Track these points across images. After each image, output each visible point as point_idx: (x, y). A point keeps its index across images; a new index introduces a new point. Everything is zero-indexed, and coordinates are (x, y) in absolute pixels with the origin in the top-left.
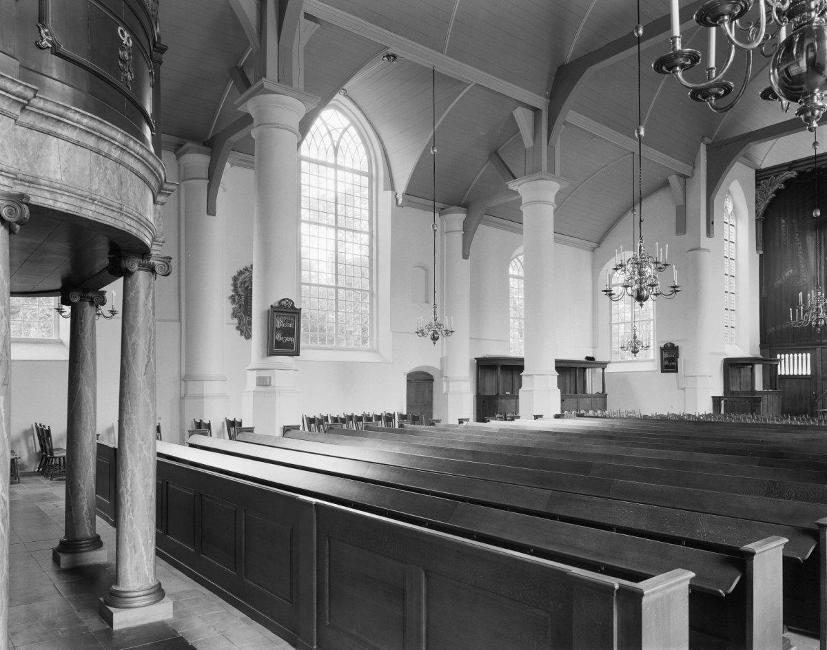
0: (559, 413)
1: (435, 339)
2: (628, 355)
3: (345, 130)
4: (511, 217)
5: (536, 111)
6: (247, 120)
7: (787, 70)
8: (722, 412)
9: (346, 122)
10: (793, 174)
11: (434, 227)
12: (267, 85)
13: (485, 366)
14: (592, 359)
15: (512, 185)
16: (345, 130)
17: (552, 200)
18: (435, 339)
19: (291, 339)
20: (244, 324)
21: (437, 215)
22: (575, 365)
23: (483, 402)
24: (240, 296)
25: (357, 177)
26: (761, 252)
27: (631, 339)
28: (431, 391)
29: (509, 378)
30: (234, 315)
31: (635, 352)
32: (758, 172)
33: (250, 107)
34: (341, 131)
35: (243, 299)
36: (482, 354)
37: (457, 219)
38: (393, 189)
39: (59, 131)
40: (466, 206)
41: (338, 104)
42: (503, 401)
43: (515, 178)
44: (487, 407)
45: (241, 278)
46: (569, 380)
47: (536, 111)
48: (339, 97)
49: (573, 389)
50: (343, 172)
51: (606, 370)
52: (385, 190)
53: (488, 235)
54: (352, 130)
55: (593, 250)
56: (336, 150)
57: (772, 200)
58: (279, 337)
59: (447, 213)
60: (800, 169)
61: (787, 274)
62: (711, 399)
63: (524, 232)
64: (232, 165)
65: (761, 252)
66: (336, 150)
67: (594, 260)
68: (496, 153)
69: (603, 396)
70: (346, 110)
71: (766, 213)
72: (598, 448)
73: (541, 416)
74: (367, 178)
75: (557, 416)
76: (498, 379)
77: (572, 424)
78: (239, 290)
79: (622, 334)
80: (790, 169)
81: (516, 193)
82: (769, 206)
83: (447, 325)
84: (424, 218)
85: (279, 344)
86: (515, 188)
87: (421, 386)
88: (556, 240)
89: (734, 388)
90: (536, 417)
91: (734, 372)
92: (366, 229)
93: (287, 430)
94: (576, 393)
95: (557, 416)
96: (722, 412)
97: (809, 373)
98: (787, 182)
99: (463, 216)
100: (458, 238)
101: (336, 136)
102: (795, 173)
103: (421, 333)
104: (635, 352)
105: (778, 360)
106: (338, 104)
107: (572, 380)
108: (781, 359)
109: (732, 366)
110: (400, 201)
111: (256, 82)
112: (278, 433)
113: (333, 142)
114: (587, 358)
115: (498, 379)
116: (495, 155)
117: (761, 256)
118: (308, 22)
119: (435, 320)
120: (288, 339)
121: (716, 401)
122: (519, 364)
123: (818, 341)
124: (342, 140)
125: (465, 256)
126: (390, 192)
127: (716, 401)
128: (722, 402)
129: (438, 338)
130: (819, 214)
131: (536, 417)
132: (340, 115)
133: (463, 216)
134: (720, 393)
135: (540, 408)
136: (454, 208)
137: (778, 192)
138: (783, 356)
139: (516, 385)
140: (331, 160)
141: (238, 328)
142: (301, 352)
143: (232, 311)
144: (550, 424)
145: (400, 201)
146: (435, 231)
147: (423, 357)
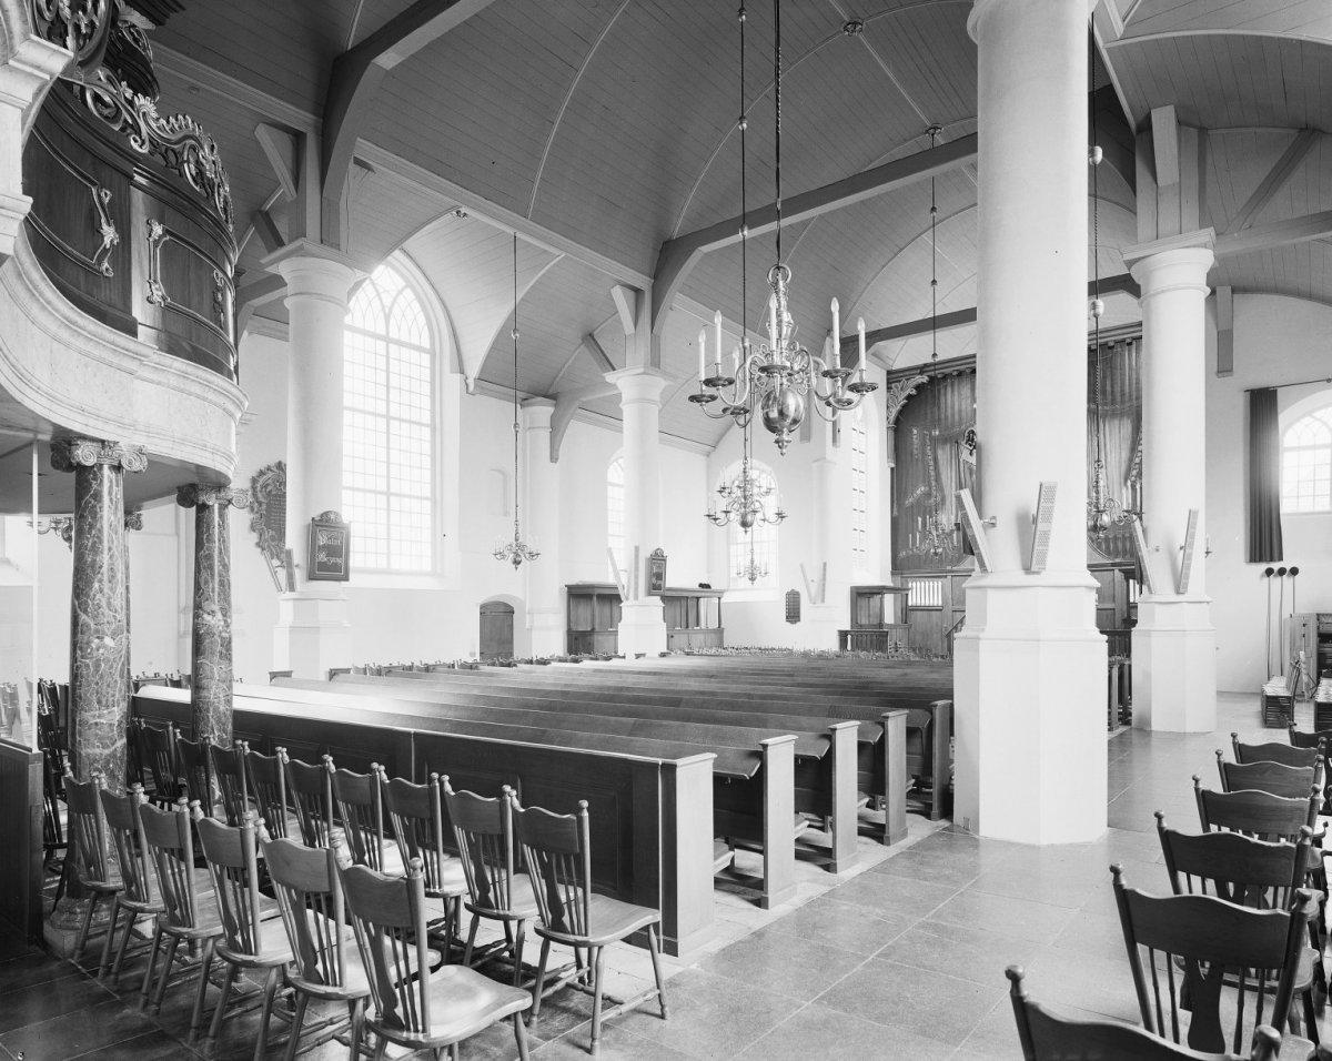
0: (665, 650)
1: (517, 562)
2: (745, 582)
3: (400, 292)
4: (609, 413)
5: (638, 291)
6: (277, 282)
7: (767, 413)
8: (849, 647)
9: (401, 283)
10: (925, 379)
11: (515, 427)
12: (306, 246)
13: (579, 595)
14: (708, 586)
15: (610, 377)
16: (400, 292)
17: (657, 398)
18: (517, 562)
19: (339, 561)
20: (266, 541)
21: (518, 406)
22: (685, 594)
23: (576, 639)
24: (260, 504)
25: (415, 354)
26: (893, 465)
27: (748, 564)
28: (511, 626)
29: (607, 610)
30: (253, 528)
31: (752, 579)
32: (889, 373)
33: (284, 269)
34: (394, 294)
35: (264, 507)
36: (574, 581)
37: (543, 411)
38: (462, 372)
39: (749, 687)
40: (552, 396)
41: (395, 263)
42: (600, 638)
43: (614, 370)
44: (579, 643)
45: (262, 480)
46: (677, 610)
47: (638, 291)
48: (397, 253)
49: (684, 623)
50: (378, 332)
51: (722, 600)
52: (452, 372)
53: (579, 431)
54: (408, 293)
55: (708, 455)
56: (387, 318)
57: (904, 406)
58: (322, 557)
59: (528, 405)
60: (929, 374)
61: (918, 492)
62: (837, 633)
63: (624, 430)
64: (250, 333)
65: (893, 465)
66: (387, 318)
67: (708, 467)
68: (591, 335)
69: (720, 631)
70: (398, 265)
71: (897, 421)
72: (694, 685)
73: (644, 655)
74: (428, 356)
75: (663, 655)
76: (591, 608)
77: (678, 662)
78: (259, 495)
79: (740, 560)
80: (921, 373)
81: (614, 386)
82: (901, 412)
83: (531, 546)
84: (499, 410)
85: (323, 566)
86: (613, 382)
87: (498, 624)
88: (661, 440)
89: (864, 621)
90: (638, 656)
91: (863, 602)
92: (426, 418)
93: (333, 674)
94: (687, 627)
95: (663, 655)
96: (849, 647)
97: (940, 604)
98: (918, 387)
99: (551, 410)
100: (545, 435)
101: (387, 301)
102: (927, 378)
103: (500, 555)
104: (752, 579)
105: (908, 590)
106: (395, 263)
107: (684, 610)
108: (912, 589)
109: (861, 595)
110: (471, 388)
111: (291, 241)
112: (323, 677)
113: (383, 307)
114: (701, 585)
115: (591, 608)
116: (590, 338)
117: (892, 469)
118: (358, 168)
119: (517, 540)
120: (333, 560)
121: (843, 635)
122: (612, 592)
123: (949, 568)
124: (396, 305)
125: (554, 459)
126: (458, 377)
127: (843, 635)
128: (849, 637)
129: (520, 563)
130: (937, 433)
131: (638, 656)
132: (392, 272)
133: (551, 410)
134: (847, 627)
135: (641, 642)
136: (539, 399)
137: (909, 397)
138: (914, 584)
139: (614, 620)
140: (393, 347)
141: (258, 544)
142: (351, 576)
143: (248, 523)
144: (653, 662)
145: (471, 388)
146: (517, 432)
147: (504, 584)
